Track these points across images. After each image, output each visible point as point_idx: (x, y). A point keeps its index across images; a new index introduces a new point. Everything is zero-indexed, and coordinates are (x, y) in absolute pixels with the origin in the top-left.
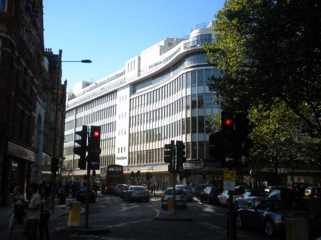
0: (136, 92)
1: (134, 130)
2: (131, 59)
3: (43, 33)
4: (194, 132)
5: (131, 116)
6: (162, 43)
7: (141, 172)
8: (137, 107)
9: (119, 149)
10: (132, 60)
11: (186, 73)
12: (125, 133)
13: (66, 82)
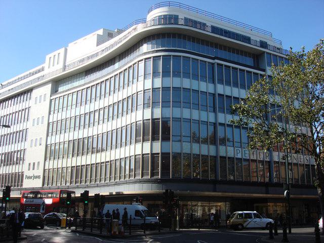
0: (57, 91)
1: (52, 140)
2: (55, 52)
4: (166, 73)
5: (51, 121)
6: (101, 32)
8: (60, 110)
9: (30, 164)
10: (56, 53)
11: (145, 59)
12: (40, 145)
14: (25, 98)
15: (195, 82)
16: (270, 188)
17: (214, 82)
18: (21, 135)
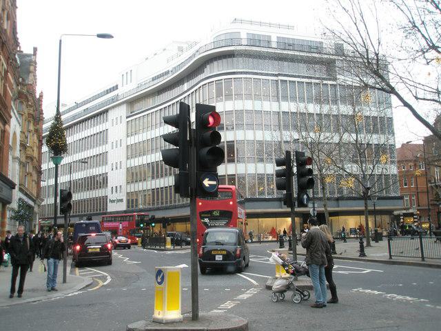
3: (15, 13)
7: (156, 217)
13: (41, 96)
14: (102, 119)
15: (302, 105)
16: (340, 202)
17: (278, 101)
18: (102, 158)
